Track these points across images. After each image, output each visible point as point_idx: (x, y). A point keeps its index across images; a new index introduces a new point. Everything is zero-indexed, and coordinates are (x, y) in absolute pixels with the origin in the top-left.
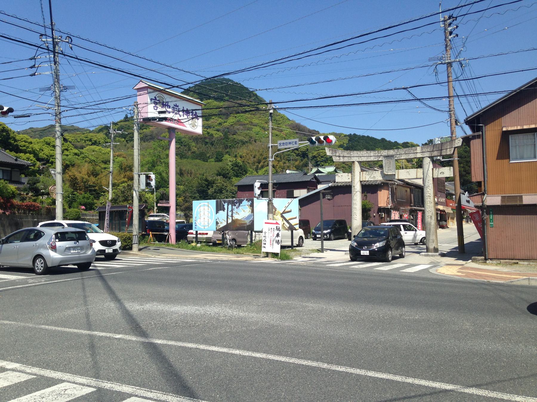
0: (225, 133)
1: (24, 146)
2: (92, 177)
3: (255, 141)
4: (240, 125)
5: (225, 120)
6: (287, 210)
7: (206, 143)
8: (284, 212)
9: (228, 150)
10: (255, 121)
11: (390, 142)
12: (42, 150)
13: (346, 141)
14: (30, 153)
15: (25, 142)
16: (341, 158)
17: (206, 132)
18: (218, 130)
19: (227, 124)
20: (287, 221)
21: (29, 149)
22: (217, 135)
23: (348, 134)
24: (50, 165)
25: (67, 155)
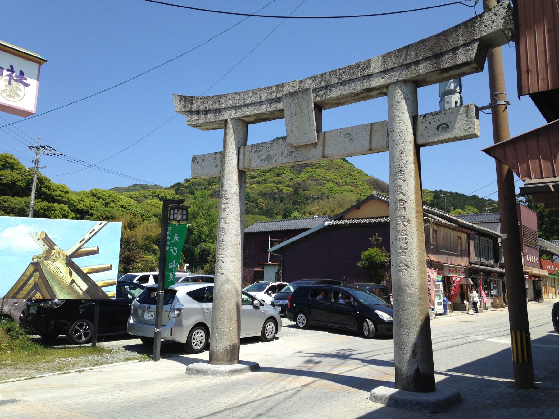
0: (296, 188)
1: (60, 196)
2: (128, 230)
3: (328, 197)
4: (312, 180)
5: (297, 176)
6: (87, 247)
7: (275, 199)
8: (77, 254)
9: (298, 206)
10: (329, 176)
11: (482, 199)
12: (83, 201)
13: (430, 198)
14: (65, 203)
15: (61, 191)
16: (202, 116)
17: (275, 188)
18: (289, 186)
19: (299, 179)
20: (84, 277)
21: (64, 199)
22: (286, 190)
23: (433, 189)
24: (90, 216)
25: (113, 207)
